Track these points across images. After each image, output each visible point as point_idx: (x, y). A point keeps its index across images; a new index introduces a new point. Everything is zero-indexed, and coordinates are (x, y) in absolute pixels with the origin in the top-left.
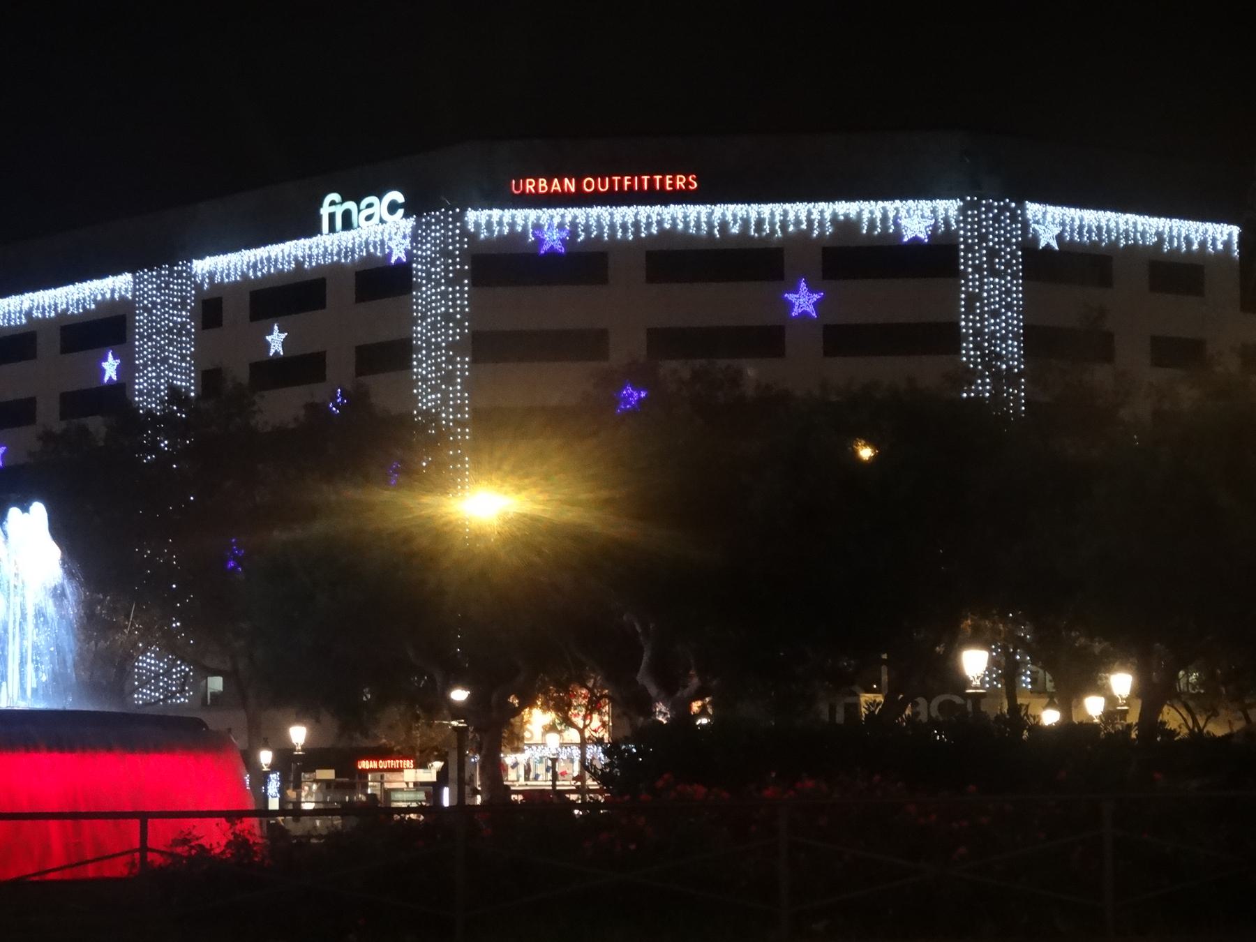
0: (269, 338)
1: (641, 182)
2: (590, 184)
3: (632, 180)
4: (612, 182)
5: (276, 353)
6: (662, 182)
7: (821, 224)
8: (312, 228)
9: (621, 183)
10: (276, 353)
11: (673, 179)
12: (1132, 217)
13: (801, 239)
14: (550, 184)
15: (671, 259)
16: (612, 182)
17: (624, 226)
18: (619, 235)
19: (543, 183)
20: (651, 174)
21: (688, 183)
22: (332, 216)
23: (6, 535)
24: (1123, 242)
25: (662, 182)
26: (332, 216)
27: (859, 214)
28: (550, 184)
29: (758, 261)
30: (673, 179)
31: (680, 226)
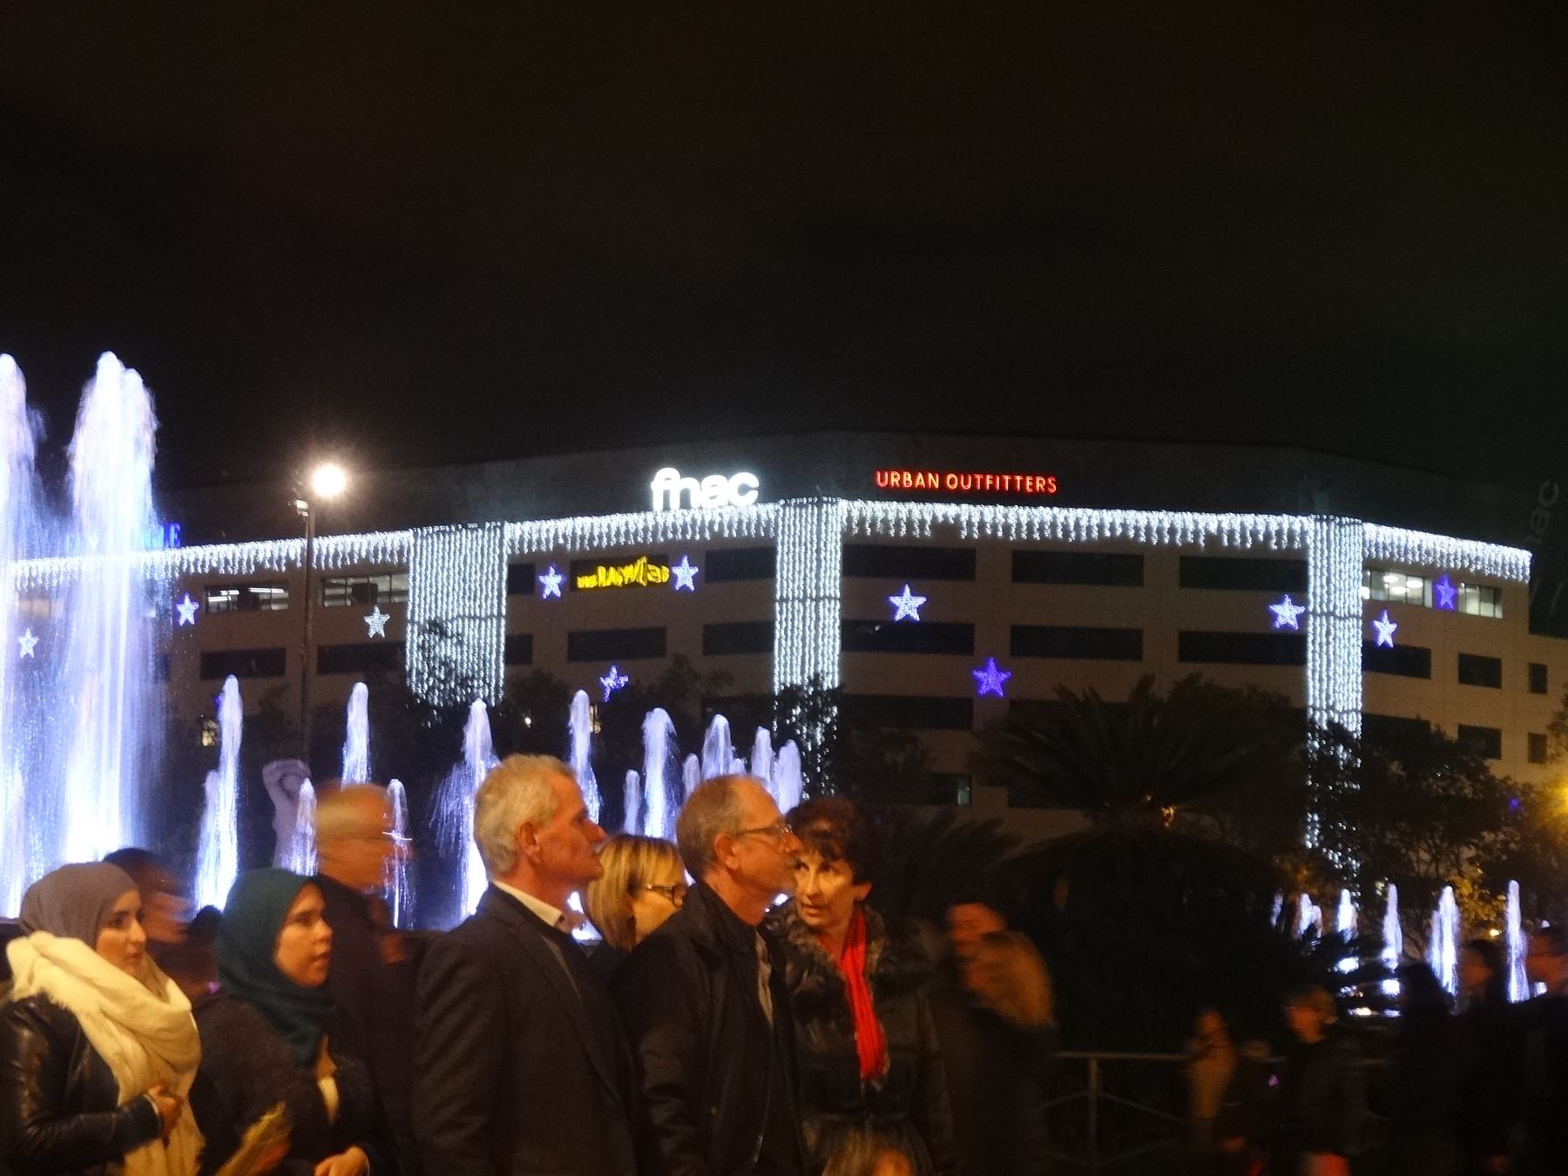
0: (368, 620)
1: (1002, 482)
2: (953, 481)
3: (994, 480)
4: (974, 481)
5: (377, 635)
6: (1023, 483)
7: (1089, 529)
8: (640, 502)
9: (983, 482)
10: (377, 635)
11: (1034, 481)
12: (1481, 545)
13: (991, 544)
14: (914, 479)
15: (1039, 561)
16: (974, 481)
17: (1231, 533)
18: (892, 533)
19: (907, 477)
20: (1012, 474)
21: (1047, 486)
22: (666, 496)
23: (777, 756)
24: (192, 570)
25: (1023, 483)
26: (666, 496)
27: (957, 518)
28: (914, 479)
29: (1117, 563)
30: (1034, 481)
31: (1132, 534)
